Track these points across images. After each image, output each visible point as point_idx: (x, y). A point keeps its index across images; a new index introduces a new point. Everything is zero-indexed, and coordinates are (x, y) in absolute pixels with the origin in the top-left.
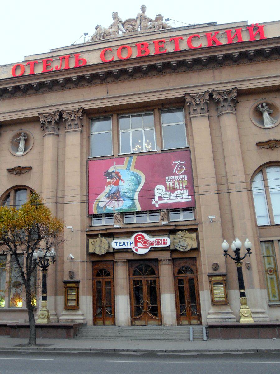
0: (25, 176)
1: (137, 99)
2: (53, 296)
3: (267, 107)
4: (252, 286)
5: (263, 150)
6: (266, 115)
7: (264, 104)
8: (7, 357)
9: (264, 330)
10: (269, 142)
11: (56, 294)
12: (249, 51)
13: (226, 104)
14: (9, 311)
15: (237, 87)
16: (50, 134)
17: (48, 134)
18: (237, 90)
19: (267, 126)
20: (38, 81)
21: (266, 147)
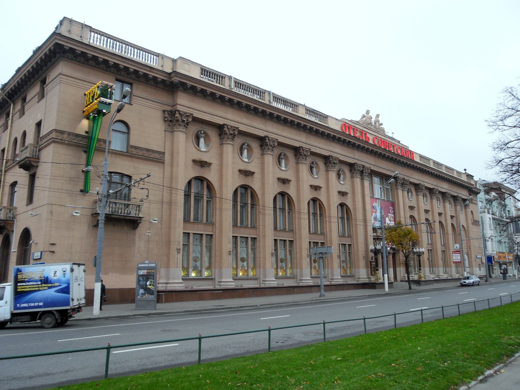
0: (206, 169)
1: (295, 144)
2: (364, 268)
3: (204, 135)
4: (424, 267)
5: (280, 183)
6: (202, 140)
7: (202, 132)
8: (57, 330)
9: (305, 289)
10: (201, 162)
11: (515, 269)
12: (198, 87)
13: (182, 124)
14: (240, 279)
15: (194, 113)
16: (368, 180)
17: (270, 154)
18: (278, 141)
19: (282, 168)
20: (222, 94)
21: (198, 164)
